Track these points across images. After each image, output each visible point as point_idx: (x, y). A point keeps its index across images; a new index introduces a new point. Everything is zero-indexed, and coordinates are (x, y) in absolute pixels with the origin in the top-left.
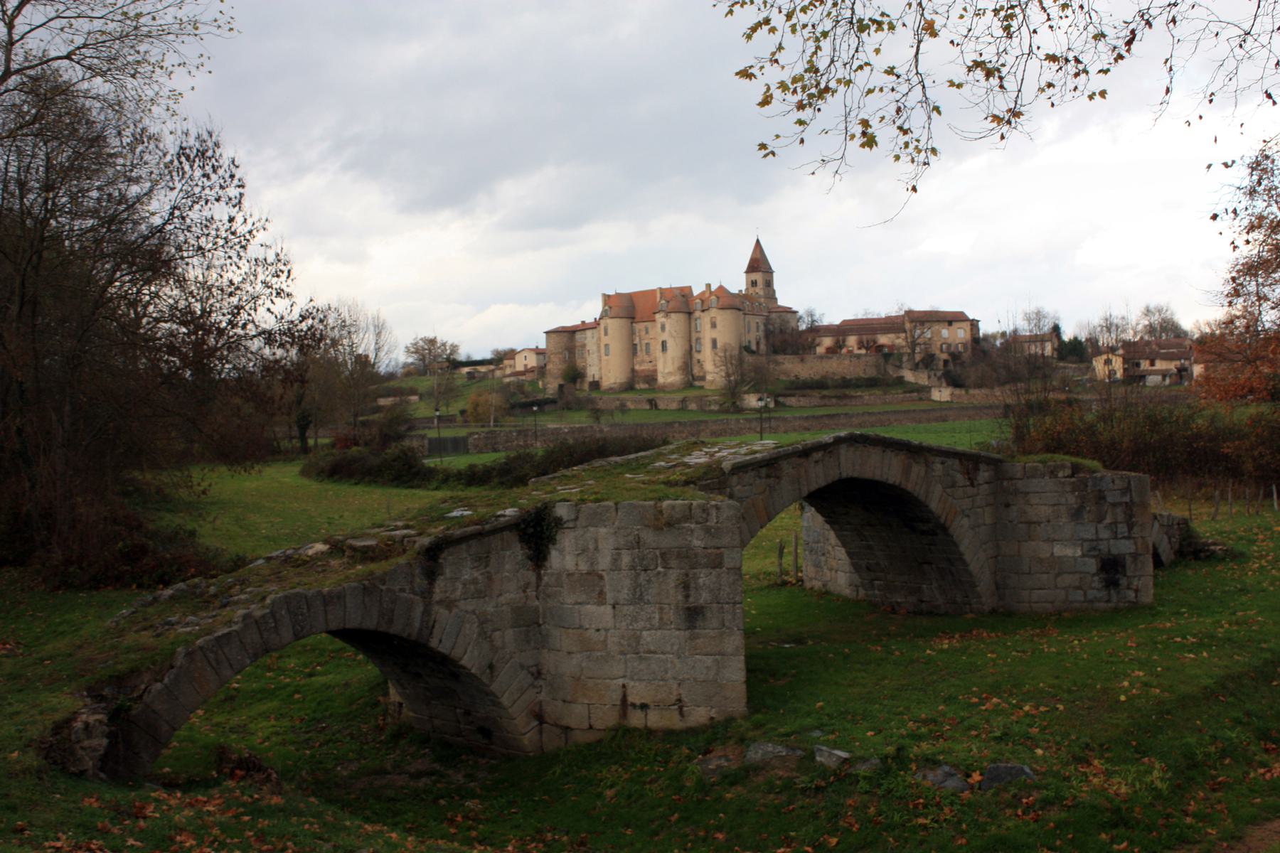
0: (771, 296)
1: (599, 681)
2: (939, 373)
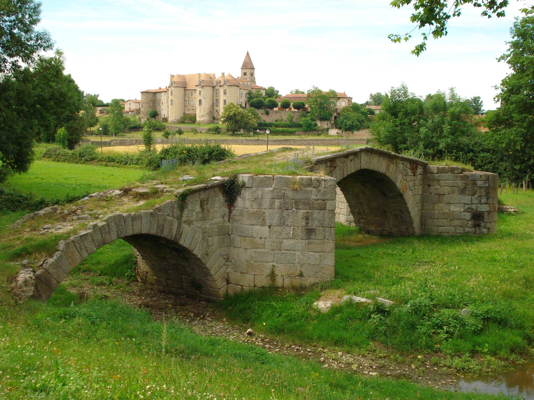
0: (253, 81)
1: (260, 263)
2: (333, 122)
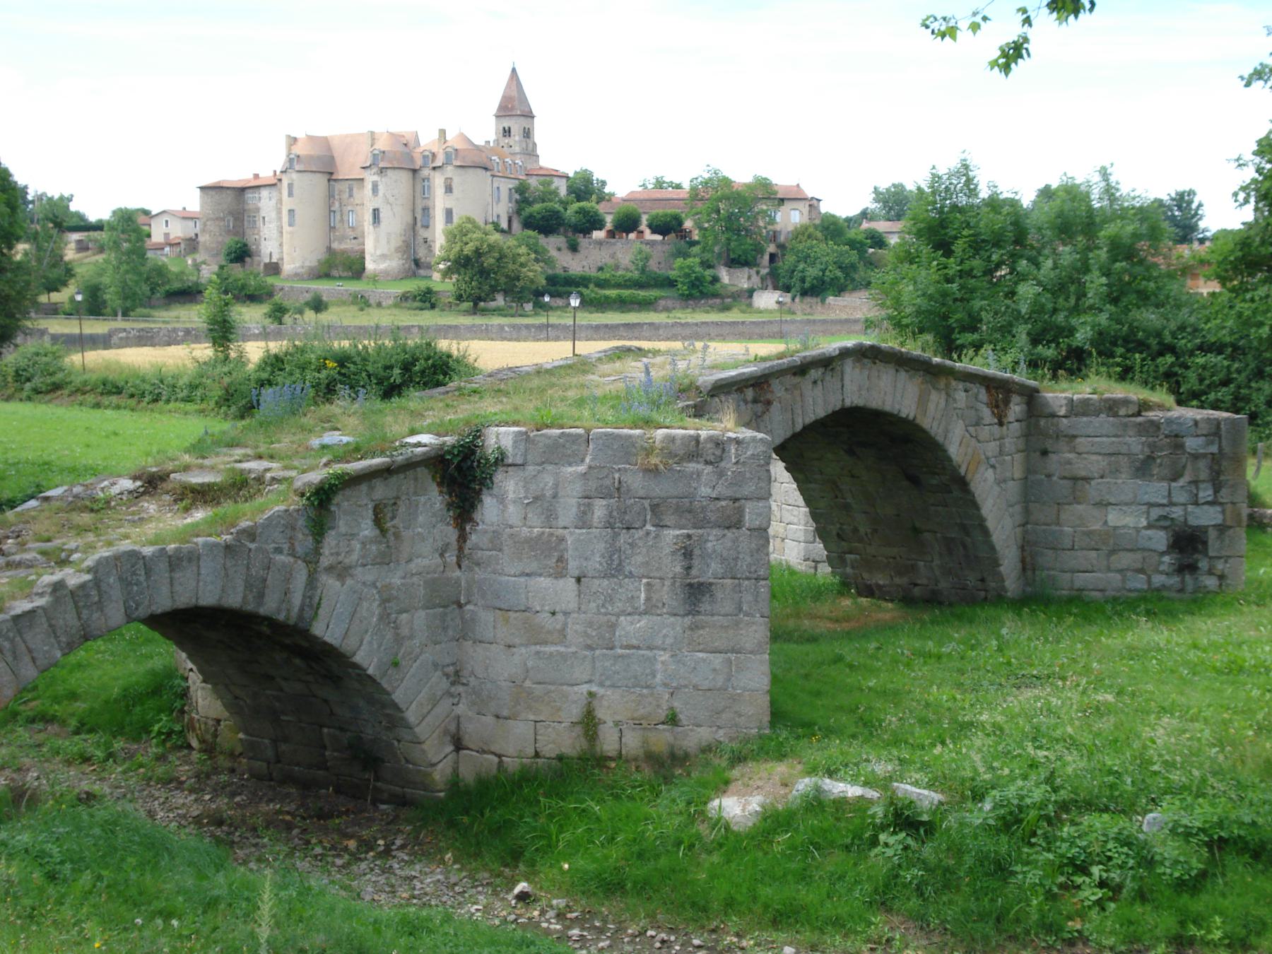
0: (531, 153)
1: (552, 688)
2: (764, 271)
